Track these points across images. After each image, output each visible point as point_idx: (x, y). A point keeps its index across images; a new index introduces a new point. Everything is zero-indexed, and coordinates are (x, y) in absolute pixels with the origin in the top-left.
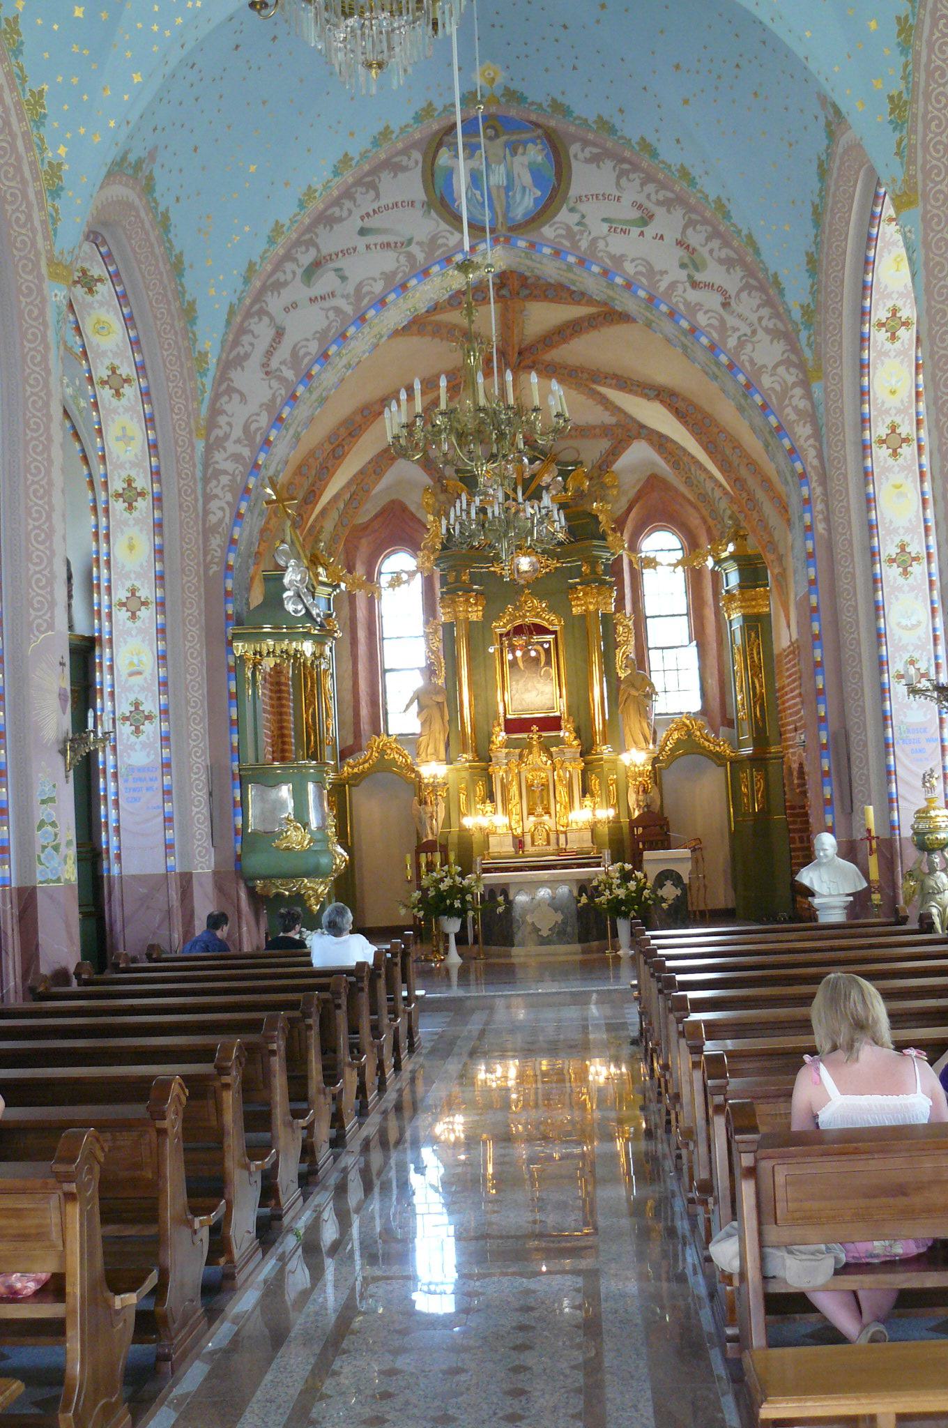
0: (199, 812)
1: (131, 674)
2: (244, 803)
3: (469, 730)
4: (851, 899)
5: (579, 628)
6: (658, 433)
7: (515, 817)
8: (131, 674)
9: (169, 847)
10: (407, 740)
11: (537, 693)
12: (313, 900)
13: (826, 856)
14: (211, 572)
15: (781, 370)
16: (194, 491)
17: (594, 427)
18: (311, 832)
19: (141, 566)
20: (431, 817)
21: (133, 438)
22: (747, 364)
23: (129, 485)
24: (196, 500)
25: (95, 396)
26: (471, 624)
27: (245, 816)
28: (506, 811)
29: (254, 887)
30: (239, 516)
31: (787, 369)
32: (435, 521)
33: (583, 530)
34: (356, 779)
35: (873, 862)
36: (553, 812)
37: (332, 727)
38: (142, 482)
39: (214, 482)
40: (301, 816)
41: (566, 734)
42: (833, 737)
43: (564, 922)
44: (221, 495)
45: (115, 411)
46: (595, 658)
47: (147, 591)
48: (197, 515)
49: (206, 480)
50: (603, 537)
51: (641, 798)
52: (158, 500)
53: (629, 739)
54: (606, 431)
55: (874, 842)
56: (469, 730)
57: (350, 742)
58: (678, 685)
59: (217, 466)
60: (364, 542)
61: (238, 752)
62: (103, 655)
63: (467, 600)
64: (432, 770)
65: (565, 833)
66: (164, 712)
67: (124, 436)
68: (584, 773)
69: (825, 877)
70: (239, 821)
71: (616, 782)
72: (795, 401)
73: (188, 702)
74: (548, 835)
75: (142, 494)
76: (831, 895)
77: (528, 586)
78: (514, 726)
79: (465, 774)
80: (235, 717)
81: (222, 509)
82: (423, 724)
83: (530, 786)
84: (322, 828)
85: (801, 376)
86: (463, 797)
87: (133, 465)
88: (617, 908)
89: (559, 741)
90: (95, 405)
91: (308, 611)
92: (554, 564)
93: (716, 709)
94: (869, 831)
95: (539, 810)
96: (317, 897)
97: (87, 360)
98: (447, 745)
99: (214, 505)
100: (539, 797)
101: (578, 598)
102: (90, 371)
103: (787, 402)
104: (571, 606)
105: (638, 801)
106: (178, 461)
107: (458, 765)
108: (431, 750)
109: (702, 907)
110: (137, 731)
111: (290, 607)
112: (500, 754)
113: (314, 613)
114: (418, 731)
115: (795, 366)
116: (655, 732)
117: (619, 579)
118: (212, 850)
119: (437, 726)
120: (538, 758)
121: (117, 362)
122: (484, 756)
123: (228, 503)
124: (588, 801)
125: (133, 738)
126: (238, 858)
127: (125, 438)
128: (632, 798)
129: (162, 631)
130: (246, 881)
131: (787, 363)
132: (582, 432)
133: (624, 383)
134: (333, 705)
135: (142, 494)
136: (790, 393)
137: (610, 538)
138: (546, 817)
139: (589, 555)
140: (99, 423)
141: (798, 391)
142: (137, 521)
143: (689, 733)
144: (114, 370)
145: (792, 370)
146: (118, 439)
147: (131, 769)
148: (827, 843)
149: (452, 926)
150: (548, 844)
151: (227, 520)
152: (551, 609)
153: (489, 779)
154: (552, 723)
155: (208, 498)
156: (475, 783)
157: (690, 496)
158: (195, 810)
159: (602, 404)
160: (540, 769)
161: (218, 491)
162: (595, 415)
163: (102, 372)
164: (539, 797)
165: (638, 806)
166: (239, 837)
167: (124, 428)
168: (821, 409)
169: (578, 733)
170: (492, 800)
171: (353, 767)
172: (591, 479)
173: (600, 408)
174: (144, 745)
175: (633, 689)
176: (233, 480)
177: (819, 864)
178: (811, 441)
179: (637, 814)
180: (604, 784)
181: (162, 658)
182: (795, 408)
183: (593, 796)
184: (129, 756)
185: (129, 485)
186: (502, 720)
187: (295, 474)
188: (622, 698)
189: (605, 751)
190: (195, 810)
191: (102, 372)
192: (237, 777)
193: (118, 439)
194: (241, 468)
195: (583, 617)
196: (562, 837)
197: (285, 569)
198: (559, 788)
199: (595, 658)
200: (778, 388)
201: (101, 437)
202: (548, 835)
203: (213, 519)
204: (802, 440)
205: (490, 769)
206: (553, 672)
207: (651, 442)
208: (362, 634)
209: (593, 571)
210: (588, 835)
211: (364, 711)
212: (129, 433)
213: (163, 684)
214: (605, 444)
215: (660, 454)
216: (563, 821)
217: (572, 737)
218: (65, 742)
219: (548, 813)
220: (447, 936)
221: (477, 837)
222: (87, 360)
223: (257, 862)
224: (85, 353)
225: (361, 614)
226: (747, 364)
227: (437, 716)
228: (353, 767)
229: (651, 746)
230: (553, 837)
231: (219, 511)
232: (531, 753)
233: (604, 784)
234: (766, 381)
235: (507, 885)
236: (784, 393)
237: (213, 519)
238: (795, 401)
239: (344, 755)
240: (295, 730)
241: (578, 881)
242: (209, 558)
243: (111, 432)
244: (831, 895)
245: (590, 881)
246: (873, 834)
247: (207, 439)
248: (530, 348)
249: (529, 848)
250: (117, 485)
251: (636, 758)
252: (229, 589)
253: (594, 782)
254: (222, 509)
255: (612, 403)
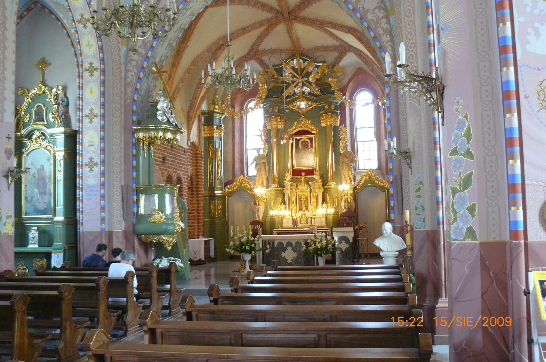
0: (117, 205)
1: (90, 146)
2: (138, 201)
3: (276, 174)
4: (398, 253)
5: (323, 131)
6: (357, 49)
7: (294, 212)
8: (90, 146)
9: (103, 220)
10: (253, 178)
11: (310, 160)
12: (167, 245)
13: (387, 233)
14: (127, 103)
15: (377, 11)
16: (120, 68)
17: (331, 47)
18: (165, 215)
19: (95, 100)
20: (258, 210)
21: (92, 45)
22: (361, 9)
23: (91, 65)
24: (121, 72)
25: (76, 28)
26: (278, 130)
27: (138, 207)
28: (290, 209)
29: (141, 238)
30: (139, 79)
31: (379, 11)
32: (262, 86)
33: (325, 89)
34: (230, 194)
35: (408, 236)
36: (309, 209)
37: (221, 171)
38: (96, 64)
39: (130, 64)
40: (162, 208)
41: (316, 176)
42: (395, 179)
43: (298, 258)
44: (132, 69)
45: (84, 34)
46: (330, 145)
47: (97, 110)
48: (121, 78)
49: (126, 64)
50: (333, 93)
51: (346, 204)
52: (103, 72)
53: (343, 179)
54: (335, 48)
55: (409, 228)
56: (276, 174)
57: (231, 178)
58: (368, 158)
59: (131, 57)
60: (239, 96)
61: (136, 180)
62: (79, 136)
63: (276, 120)
64: (260, 191)
65: (314, 218)
66: (103, 162)
67: (89, 44)
68: (324, 193)
69: (386, 243)
70: (135, 209)
71: (337, 197)
72: (382, 25)
73: (113, 158)
74: (307, 219)
75: (96, 69)
76: (388, 251)
77: (303, 114)
78: (296, 173)
79: (273, 193)
80: (135, 165)
81: (132, 76)
82: (257, 171)
83: (300, 200)
84: (173, 213)
85: (385, 13)
86: (272, 202)
87: (93, 57)
88: (318, 252)
89: (314, 180)
90: (76, 31)
91: (168, 120)
92: (314, 105)
93: (383, 169)
94: (407, 222)
95: (304, 209)
96: (169, 243)
97: (71, 12)
98: (268, 180)
99: (129, 74)
100: (303, 204)
101: (323, 119)
102: (73, 17)
103: (379, 25)
104: (321, 123)
105: (345, 206)
106: (112, 55)
107: (270, 189)
108: (260, 182)
109: (365, 252)
110: (91, 170)
111: (160, 118)
112: (288, 184)
113: (171, 120)
114: (255, 175)
115: (383, 9)
116: (355, 177)
117: (342, 112)
118: (124, 222)
119: (263, 173)
120: (304, 187)
121: (83, 13)
122: (281, 185)
123: (135, 73)
124: (325, 205)
125: (89, 173)
126: (134, 225)
127: (89, 45)
128: (343, 204)
129: (103, 128)
130: (137, 235)
131: (379, 8)
132: (326, 49)
133: (335, 26)
134: (221, 164)
135: (96, 69)
136: (380, 21)
137: (336, 94)
138: (307, 212)
139: (329, 100)
140: (79, 39)
141: (384, 21)
142: (94, 81)
143: (370, 178)
144: (82, 16)
145: (381, 11)
146: (86, 46)
147: (88, 186)
148: (388, 226)
149: (248, 257)
150: (307, 223)
151: (134, 80)
152: (313, 124)
153: (284, 195)
154: (310, 172)
155: (127, 71)
156: (277, 197)
157: (374, 76)
158: (115, 204)
159: (332, 37)
160: (304, 191)
161: (131, 68)
162: (331, 42)
163: (78, 17)
164: (303, 204)
165: (345, 208)
166: (135, 216)
167: (88, 41)
168: (394, 29)
169: (322, 177)
170: (285, 204)
171: (229, 189)
172: (328, 68)
173: (331, 38)
174: (94, 176)
175: (347, 158)
176: (137, 63)
177: (384, 237)
178: (389, 43)
179: (344, 211)
180: (332, 199)
181: (103, 139)
182: (382, 28)
183: (327, 203)
184: (88, 181)
185: (91, 65)
186: (290, 170)
187: (191, 65)
188: (341, 162)
189: (332, 184)
190: (115, 204)
191: (78, 17)
192: (134, 190)
193: (86, 46)
194: (141, 58)
195: (325, 127)
196: (313, 220)
197: (158, 102)
198: (313, 199)
199: (330, 145)
200: (375, 19)
201: (80, 45)
202: (307, 219)
203: (129, 80)
204: (385, 43)
205: (284, 191)
206: (314, 150)
207: (356, 54)
208: (237, 134)
209: (330, 108)
210: (324, 220)
211: (237, 166)
212: (91, 43)
213: (103, 150)
214: (335, 54)
215: (359, 58)
216: (314, 214)
217: (318, 178)
218: (8, 172)
219: (307, 210)
220: (245, 261)
221: (277, 220)
222: (71, 12)
223: (141, 228)
224: (70, 9)
225: (237, 125)
226: (361, 9)
227: (263, 167)
228: (229, 189)
229: (353, 183)
230: (309, 220)
231: (131, 77)
232: (301, 184)
233: (332, 199)
234: (370, 16)
235: (274, 240)
236: (377, 22)
237: (129, 80)
238: (382, 25)
239: (226, 184)
240: (204, 173)
241: (304, 239)
242: (126, 97)
243: (84, 43)
244: (388, 251)
245: (308, 240)
246: (408, 223)
247: (127, 46)
248: (293, 10)
249: (299, 225)
250: (86, 65)
251: (345, 188)
252: (135, 110)
253: (328, 198)
254: (132, 76)
255: (336, 36)
